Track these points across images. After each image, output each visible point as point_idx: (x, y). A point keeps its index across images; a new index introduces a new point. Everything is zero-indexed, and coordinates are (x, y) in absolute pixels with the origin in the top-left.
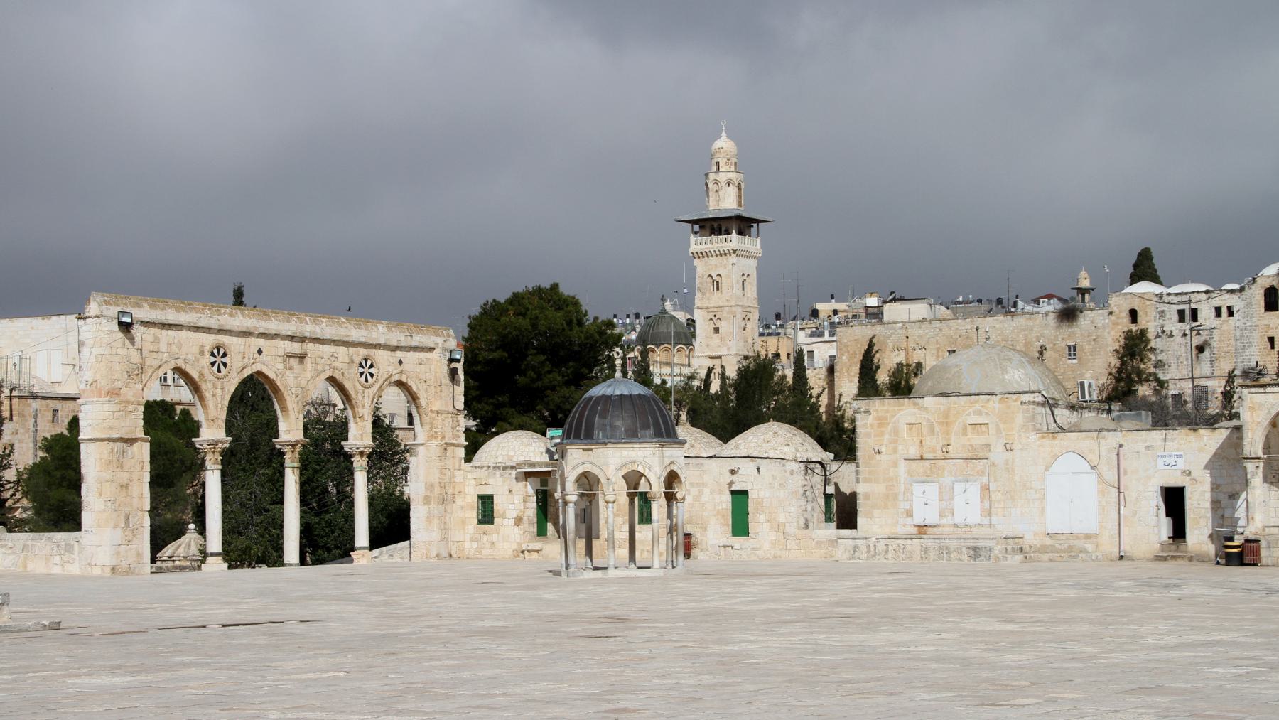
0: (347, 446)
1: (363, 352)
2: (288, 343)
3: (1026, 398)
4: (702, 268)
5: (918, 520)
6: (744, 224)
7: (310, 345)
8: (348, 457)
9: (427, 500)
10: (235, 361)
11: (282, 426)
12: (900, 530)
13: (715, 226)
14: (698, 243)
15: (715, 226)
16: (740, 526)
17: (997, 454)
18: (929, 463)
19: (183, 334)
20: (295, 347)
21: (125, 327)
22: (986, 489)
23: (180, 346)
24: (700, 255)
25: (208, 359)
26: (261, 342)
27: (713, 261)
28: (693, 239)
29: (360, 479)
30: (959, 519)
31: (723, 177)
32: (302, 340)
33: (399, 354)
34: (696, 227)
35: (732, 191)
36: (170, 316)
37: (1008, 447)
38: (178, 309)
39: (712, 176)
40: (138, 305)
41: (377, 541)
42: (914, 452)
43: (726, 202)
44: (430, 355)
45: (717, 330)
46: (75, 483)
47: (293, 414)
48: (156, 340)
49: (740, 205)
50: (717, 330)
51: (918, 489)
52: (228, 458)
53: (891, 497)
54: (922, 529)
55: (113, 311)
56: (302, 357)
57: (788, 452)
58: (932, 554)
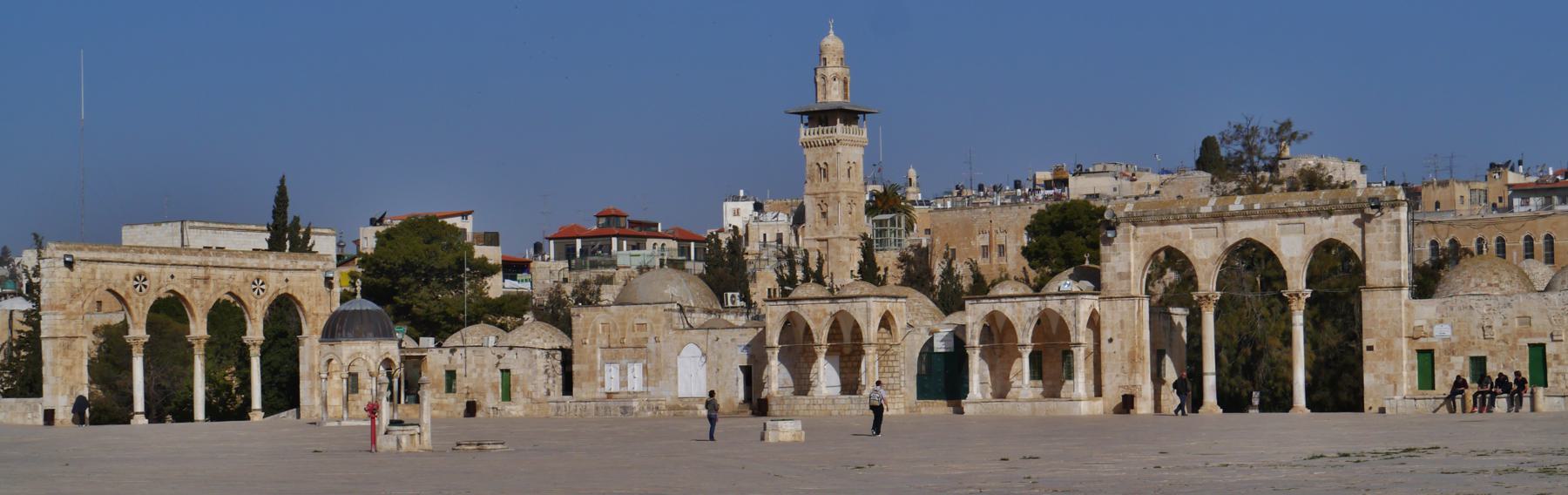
0: (246, 339)
1: (256, 274)
2: (195, 270)
3: (668, 306)
4: (810, 155)
5: (607, 389)
6: (850, 116)
7: (213, 271)
8: (1286, 302)
9: (310, 377)
10: (152, 284)
11: (192, 326)
12: (598, 396)
13: (823, 117)
14: (805, 134)
15: (823, 117)
16: (507, 396)
17: (651, 345)
18: (615, 351)
19: (114, 266)
20: (201, 272)
21: (69, 265)
22: (645, 368)
23: (111, 274)
24: (808, 145)
25: (132, 283)
26: (173, 270)
27: (820, 150)
28: (802, 129)
29: (255, 364)
30: (630, 388)
31: (830, 72)
32: (206, 266)
33: (286, 275)
34: (806, 119)
35: (838, 84)
36: (104, 255)
37: (657, 341)
38: (110, 251)
39: (819, 71)
40: (80, 249)
41: (269, 409)
42: (605, 343)
43: (834, 95)
44: (313, 274)
45: (824, 214)
46: (36, 360)
47: (198, 319)
48: (93, 271)
49: (846, 97)
50: (824, 214)
51: (607, 367)
52: (150, 351)
53: (592, 374)
54: (610, 395)
55: (61, 254)
56: (206, 279)
57: (539, 343)
58: (602, 411)
